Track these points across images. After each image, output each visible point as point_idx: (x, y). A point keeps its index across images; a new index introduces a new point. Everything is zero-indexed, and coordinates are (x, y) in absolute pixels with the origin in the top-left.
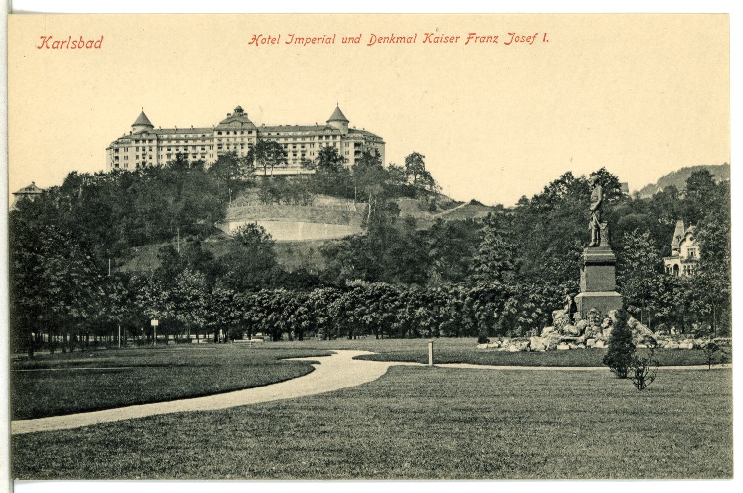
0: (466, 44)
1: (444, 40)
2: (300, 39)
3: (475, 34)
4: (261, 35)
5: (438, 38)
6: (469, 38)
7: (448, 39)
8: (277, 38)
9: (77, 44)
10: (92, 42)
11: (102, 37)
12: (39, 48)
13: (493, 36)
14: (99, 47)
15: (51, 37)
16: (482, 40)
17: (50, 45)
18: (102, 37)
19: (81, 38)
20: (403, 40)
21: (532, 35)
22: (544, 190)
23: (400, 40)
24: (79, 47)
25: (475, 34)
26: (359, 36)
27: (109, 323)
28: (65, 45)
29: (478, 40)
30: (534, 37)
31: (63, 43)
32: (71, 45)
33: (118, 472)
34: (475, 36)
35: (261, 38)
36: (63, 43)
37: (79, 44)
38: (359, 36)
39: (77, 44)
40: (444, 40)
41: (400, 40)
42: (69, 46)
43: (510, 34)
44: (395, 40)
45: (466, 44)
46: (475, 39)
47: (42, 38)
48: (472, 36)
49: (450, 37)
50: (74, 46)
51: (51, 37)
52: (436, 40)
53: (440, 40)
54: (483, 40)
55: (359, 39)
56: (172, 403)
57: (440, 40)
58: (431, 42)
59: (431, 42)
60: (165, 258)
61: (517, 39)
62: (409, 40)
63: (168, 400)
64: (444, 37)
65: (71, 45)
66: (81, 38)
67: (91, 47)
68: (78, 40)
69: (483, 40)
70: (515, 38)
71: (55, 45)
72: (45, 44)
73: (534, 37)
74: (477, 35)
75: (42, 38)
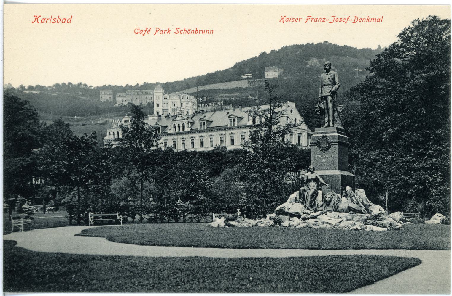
0: (306, 22)
2: (374, 19)
3: (311, 16)
4: (285, 16)
6: (307, 19)
7: (294, 20)
9: (56, 20)
10: (65, 19)
12: (33, 22)
14: (70, 22)
15: (40, 16)
16: (316, 20)
17: (39, 21)
20: (374, 20)
21: (346, 18)
23: (372, 20)
24: (57, 22)
25: (311, 16)
26: (70, 18)
28: (49, 21)
29: (313, 20)
30: (348, 19)
31: (47, 19)
32: (52, 20)
33: (222, 290)
34: (311, 18)
35: (285, 18)
37: (56, 21)
38: (70, 18)
39: (56, 20)
40: (292, 20)
41: (372, 20)
42: (51, 22)
43: (332, 16)
44: (370, 20)
45: (306, 22)
46: (311, 19)
47: (34, 16)
48: (309, 18)
51: (40, 16)
53: (289, 20)
54: (316, 20)
55: (71, 19)
56: (358, 250)
57: (289, 20)
58: (38, 22)
59: (38, 22)
63: (432, 249)
64: (292, 18)
65: (52, 20)
68: (57, 18)
69: (316, 20)
71: (43, 21)
72: (36, 20)
73: (348, 19)
74: (312, 17)
75: (34, 16)
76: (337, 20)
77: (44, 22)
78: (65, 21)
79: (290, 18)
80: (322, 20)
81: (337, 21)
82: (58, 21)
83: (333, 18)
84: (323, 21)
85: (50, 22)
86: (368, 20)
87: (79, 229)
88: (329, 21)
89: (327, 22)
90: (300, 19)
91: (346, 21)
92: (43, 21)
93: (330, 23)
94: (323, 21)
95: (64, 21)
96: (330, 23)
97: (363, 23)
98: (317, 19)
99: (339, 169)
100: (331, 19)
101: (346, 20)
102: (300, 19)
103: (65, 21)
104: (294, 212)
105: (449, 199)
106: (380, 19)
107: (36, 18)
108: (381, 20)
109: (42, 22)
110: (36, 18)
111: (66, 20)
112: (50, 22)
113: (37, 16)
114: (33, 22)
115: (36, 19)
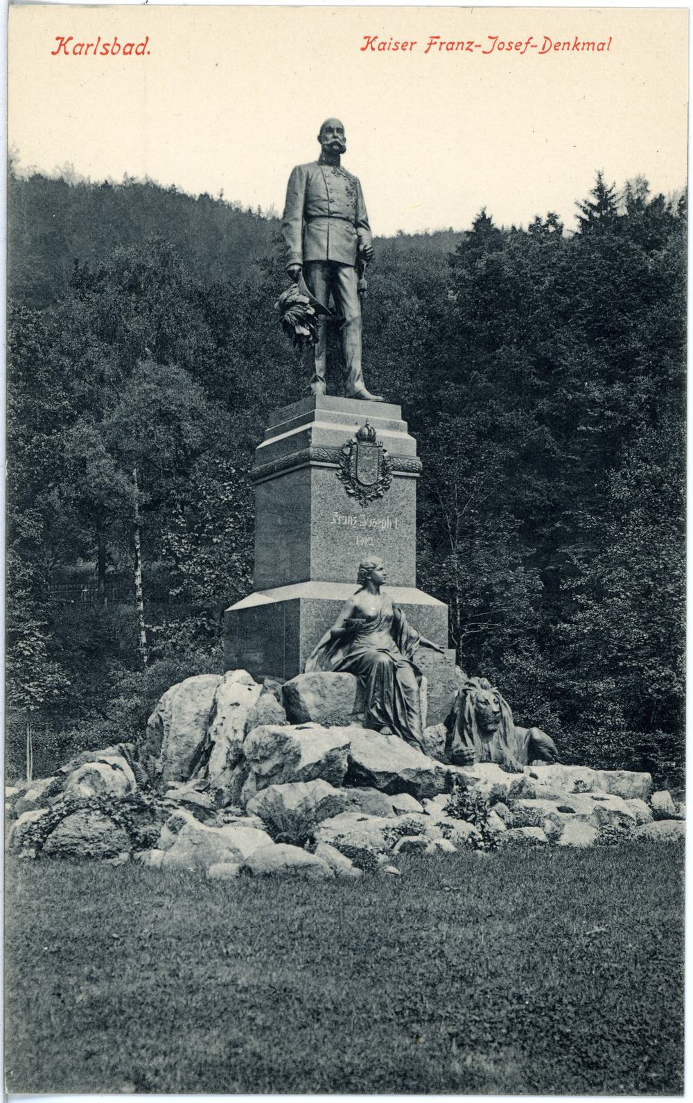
0: (426, 52)
1: (393, 46)
3: (438, 37)
5: (385, 44)
6: (430, 44)
8: (607, 41)
10: (132, 45)
11: (147, 39)
13: (465, 42)
16: (450, 46)
18: (147, 39)
19: (116, 39)
22: (510, 228)
23: (586, 46)
25: (438, 37)
26: (144, 41)
27: (649, 241)
28: (92, 49)
29: (444, 47)
30: (527, 43)
31: (88, 46)
32: (100, 49)
34: (438, 41)
36: (88, 46)
38: (144, 41)
39: (109, 48)
41: (586, 46)
42: (98, 52)
44: (580, 47)
45: (426, 52)
46: (438, 44)
47: (365, 38)
48: (434, 40)
49: (515, 43)
50: (104, 51)
51: (71, 38)
52: (382, 46)
54: (451, 46)
55: (144, 45)
57: (387, 46)
58: (66, 53)
59: (66, 53)
60: (583, 220)
61: (501, 46)
62: (601, 47)
66: (116, 39)
67: (130, 53)
68: (112, 42)
69: (451, 46)
70: (498, 44)
71: (77, 50)
72: (62, 48)
73: (527, 43)
76: (501, 46)
77: (80, 53)
78: (129, 49)
79: (388, 41)
80: (466, 46)
81: (500, 49)
82: (115, 51)
83: (492, 41)
84: (467, 49)
85: (95, 53)
86: (575, 45)
87: (295, 726)
88: (481, 50)
89: (477, 51)
90: (412, 44)
91: (522, 48)
92: (77, 50)
93: (484, 52)
94: (467, 49)
95: (128, 49)
96: (484, 52)
97: (563, 54)
98: (453, 44)
99: (419, 585)
100: (487, 45)
101: (524, 46)
102: (412, 44)
103: (129, 49)
104: (408, 771)
105: (297, 1091)
106: (603, 44)
107: (369, 40)
108: (606, 47)
109: (75, 53)
110: (369, 40)
111: (134, 47)
112: (95, 53)
113: (63, 39)
114: (54, 53)
115: (61, 45)
